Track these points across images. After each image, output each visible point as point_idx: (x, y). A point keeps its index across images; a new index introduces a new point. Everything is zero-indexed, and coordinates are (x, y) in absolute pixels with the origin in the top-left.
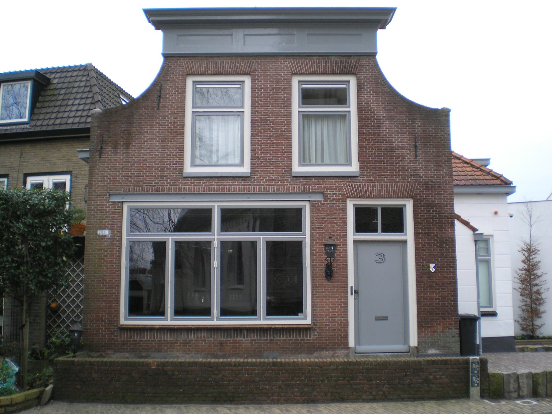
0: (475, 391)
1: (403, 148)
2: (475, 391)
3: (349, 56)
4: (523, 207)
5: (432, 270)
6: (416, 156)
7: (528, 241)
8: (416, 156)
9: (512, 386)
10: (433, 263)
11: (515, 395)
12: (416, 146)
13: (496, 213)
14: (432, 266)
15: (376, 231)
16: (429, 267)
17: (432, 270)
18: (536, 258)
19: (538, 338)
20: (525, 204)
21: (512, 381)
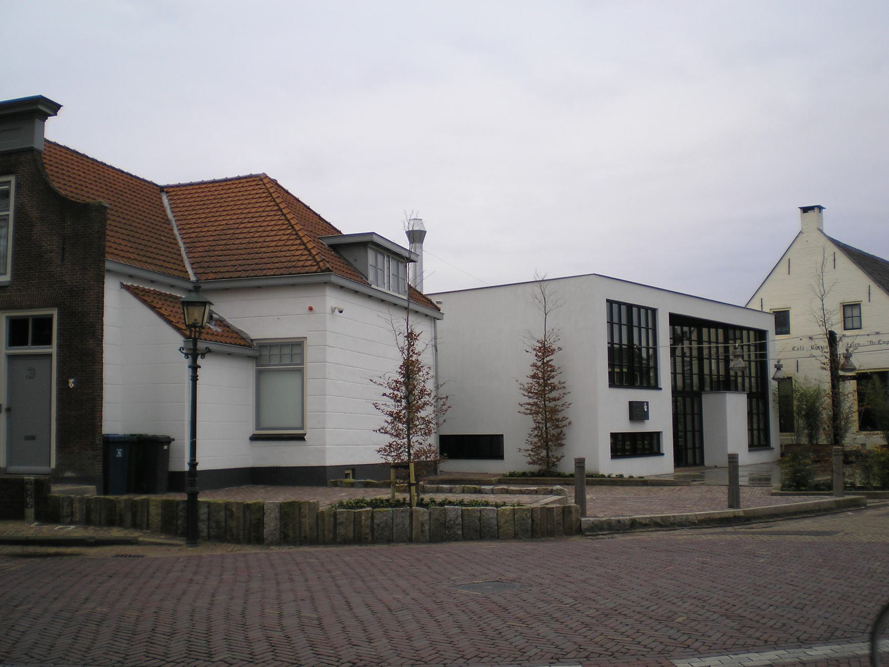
0: (30, 512)
1: (51, 252)
2: (30, 512)
3: (10, 153)
4: (536, 289)
5: (71, 385)
6: (63, 260)
7: (541, 337)
8: (63, 260)
9: (66, 511)
10: (72, 378)
11: (69, 519)
12: (63, 249)
13: (311, 309)
14: (71, 381)
15: (26, 344)
16: (68, 383)
17: (71, 385)
18: (555, 360)
19: (559, 475)
20: (536, 284)
21: (65, 504)
